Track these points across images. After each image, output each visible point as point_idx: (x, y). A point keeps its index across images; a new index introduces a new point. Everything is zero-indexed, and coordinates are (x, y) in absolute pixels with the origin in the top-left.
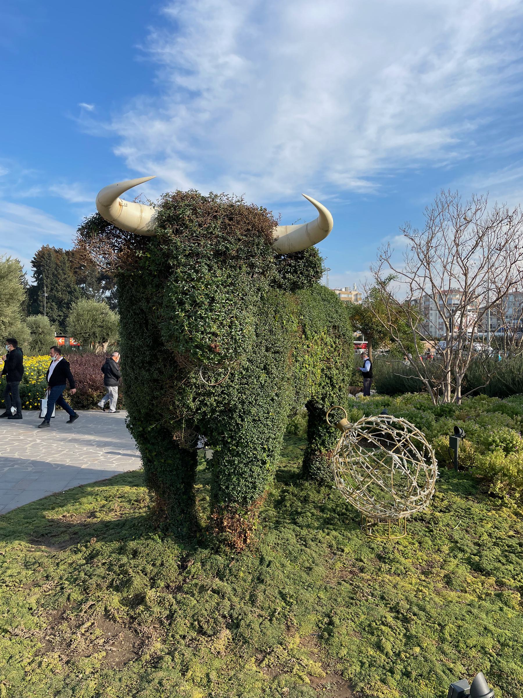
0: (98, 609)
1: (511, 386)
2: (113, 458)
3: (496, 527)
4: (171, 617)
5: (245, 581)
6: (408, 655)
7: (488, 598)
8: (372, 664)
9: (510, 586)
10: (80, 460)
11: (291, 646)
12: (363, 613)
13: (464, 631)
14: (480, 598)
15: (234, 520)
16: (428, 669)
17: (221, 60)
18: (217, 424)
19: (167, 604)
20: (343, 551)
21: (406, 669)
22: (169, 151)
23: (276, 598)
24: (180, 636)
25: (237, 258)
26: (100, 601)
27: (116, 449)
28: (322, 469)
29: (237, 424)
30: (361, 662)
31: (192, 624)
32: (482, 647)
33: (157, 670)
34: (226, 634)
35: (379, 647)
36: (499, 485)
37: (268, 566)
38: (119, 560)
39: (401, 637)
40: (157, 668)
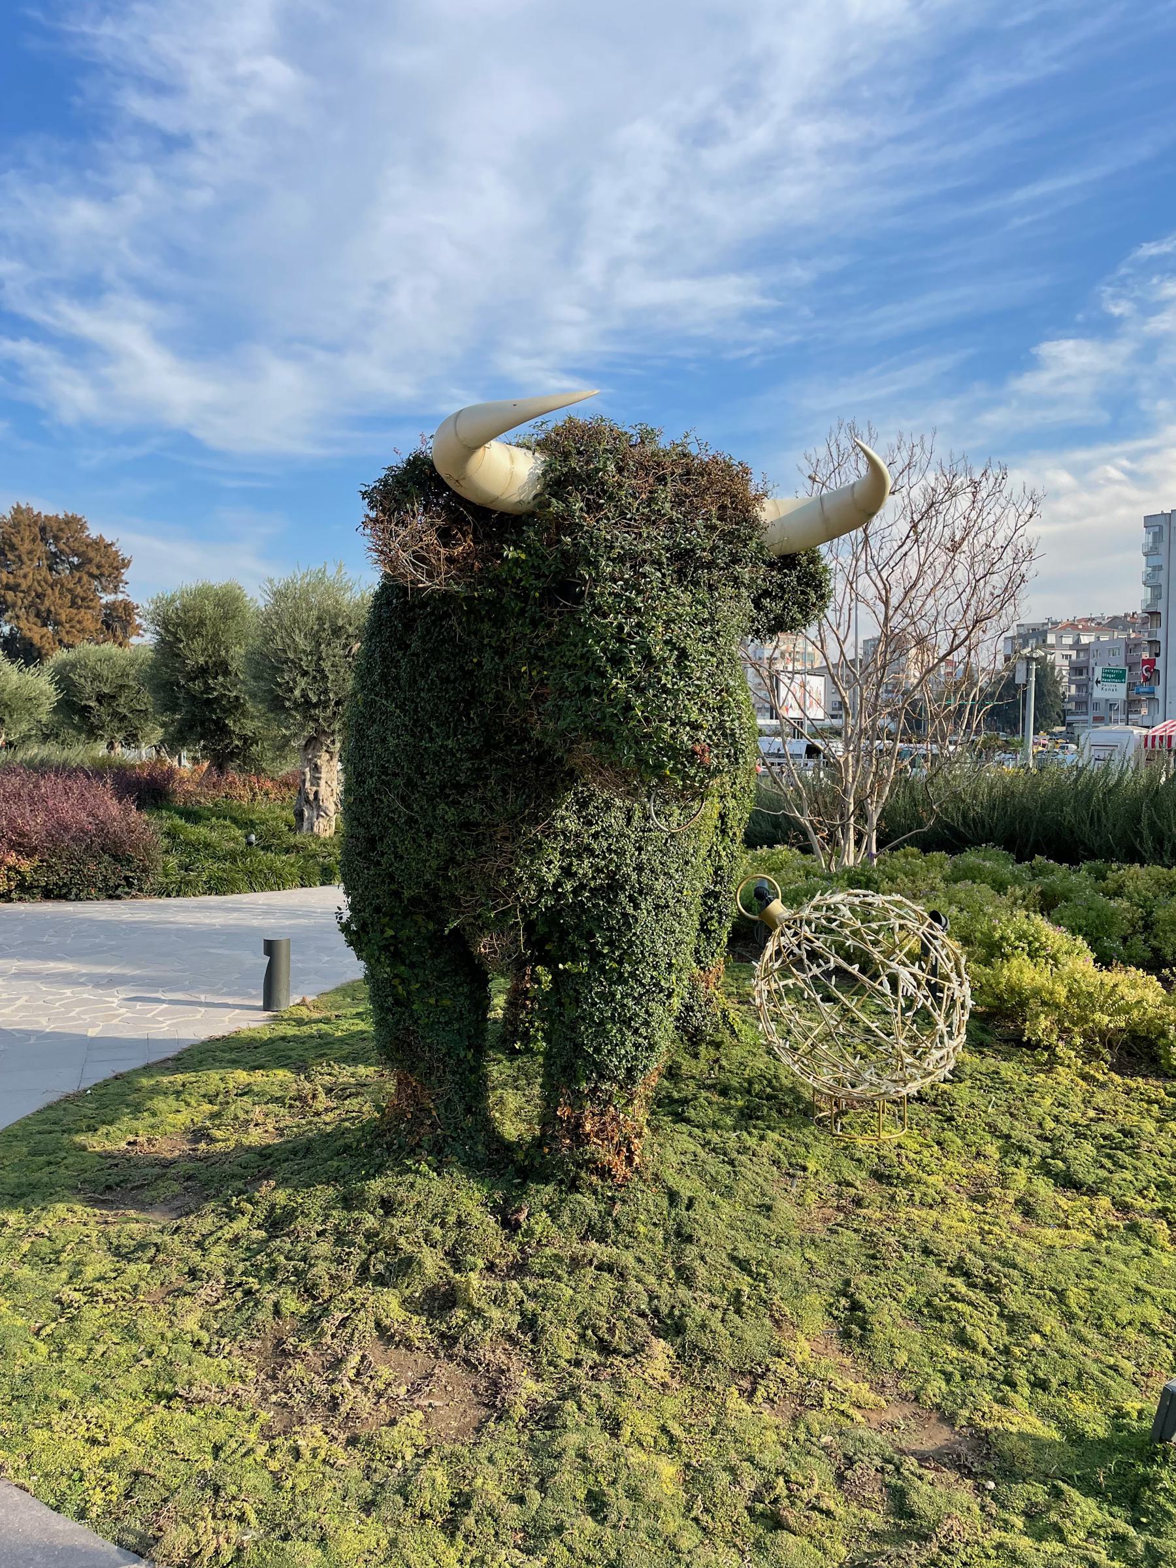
0: (361, 1327)
1: (962, 829)
2: (153, 1010)
3: (1060, 1105)
4: (529, 1323)
5: (652, 1241)
6: (1026, 1352)
7: (1114, 1235)
8: (967, 1374)
9: (1142, 1209)
10: (74, 1019)
11: (799, 1359)
12: (907, 1282)
13: (1104, 1297)
14: (1099, 1236)
15: (607, 1118)
16: (1074, 1371)
17: (243, 67)
18: (579, 917)
19: (512, 1299)
20: (804, 1169)
21: (1035, 1375)
22: (110, 274)
23: (728, 1268)
24: (569, 1362)
25: (710, 565)
26: (359, 1310)
27: (145, 992)
28: (696, 1008)
29: (625, 915)
30: (943, 1372)
31: (583, 1336)
32: (1143, 1324)
33: (557, 1431)
34: (660, 1347)
35: (963, 1340)
36: (1044, 1023)
37: (688, 1209)
38: (358, 1222)
39: (995, 1318)
40: (554, 1427)
